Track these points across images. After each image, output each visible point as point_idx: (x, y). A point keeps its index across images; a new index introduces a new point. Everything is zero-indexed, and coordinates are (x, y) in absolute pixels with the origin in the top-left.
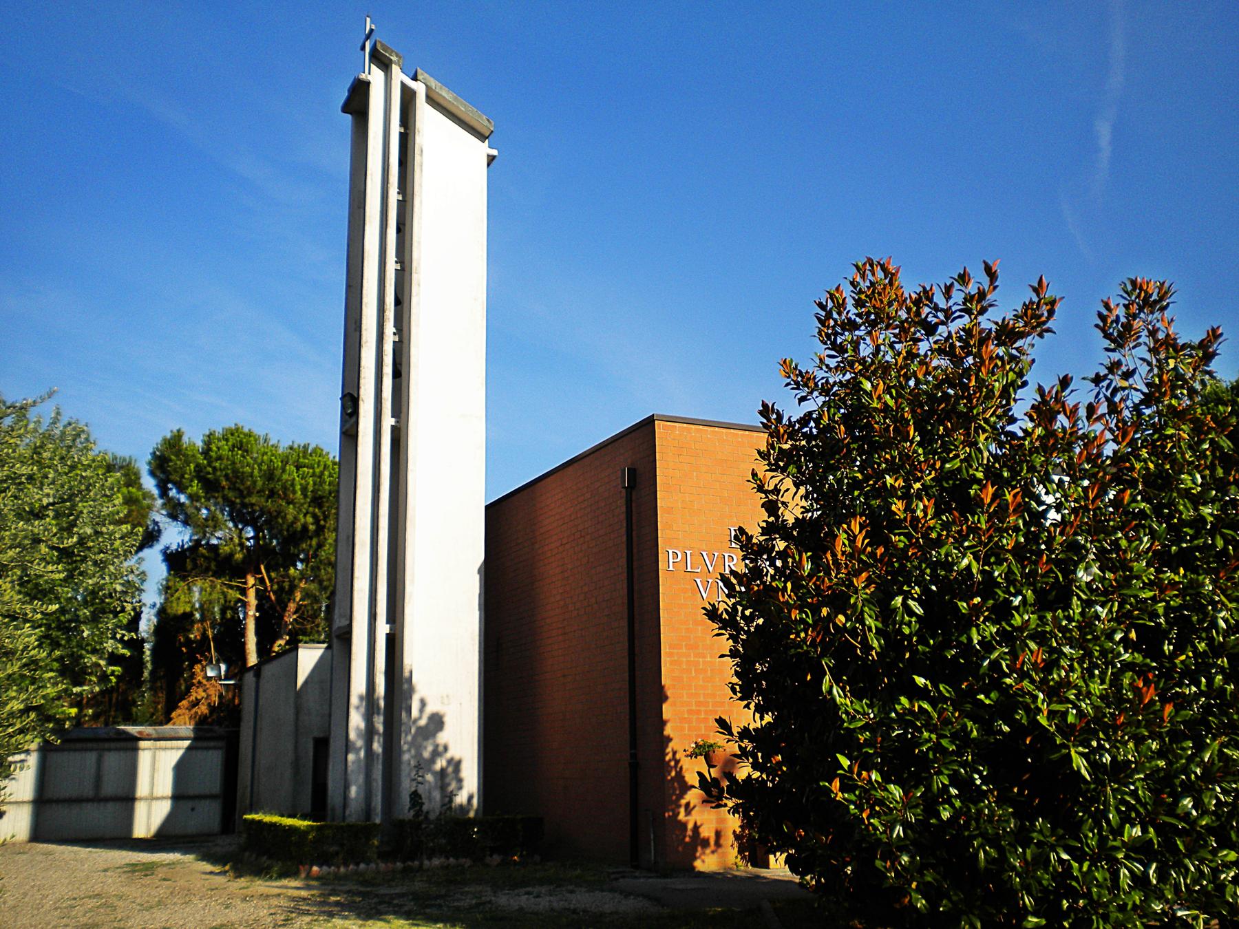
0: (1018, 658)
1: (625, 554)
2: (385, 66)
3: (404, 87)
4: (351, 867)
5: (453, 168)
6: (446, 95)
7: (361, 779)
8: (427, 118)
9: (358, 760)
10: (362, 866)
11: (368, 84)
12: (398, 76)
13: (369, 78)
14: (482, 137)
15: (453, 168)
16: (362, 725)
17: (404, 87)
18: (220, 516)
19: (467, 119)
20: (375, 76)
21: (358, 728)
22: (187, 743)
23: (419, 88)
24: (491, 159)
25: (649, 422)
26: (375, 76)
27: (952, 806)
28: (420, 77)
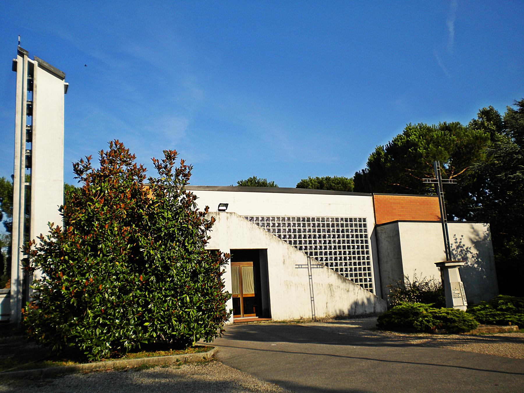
0: (76, 335)
2: (22, 55)
4: (4, 338)
7: (15, 308)
8: (40, 74)
9: (14, 302)
10: (8, 338)
14: (62, 78)
15: (50, 90)
16: (16, 289)
18: (110, 257)
20: (19, 59)
21: (14, 291)
22: (5, 295)
23: (35, 63)
24: (66, 87)
26: (19, 59)
27: (122, 226)
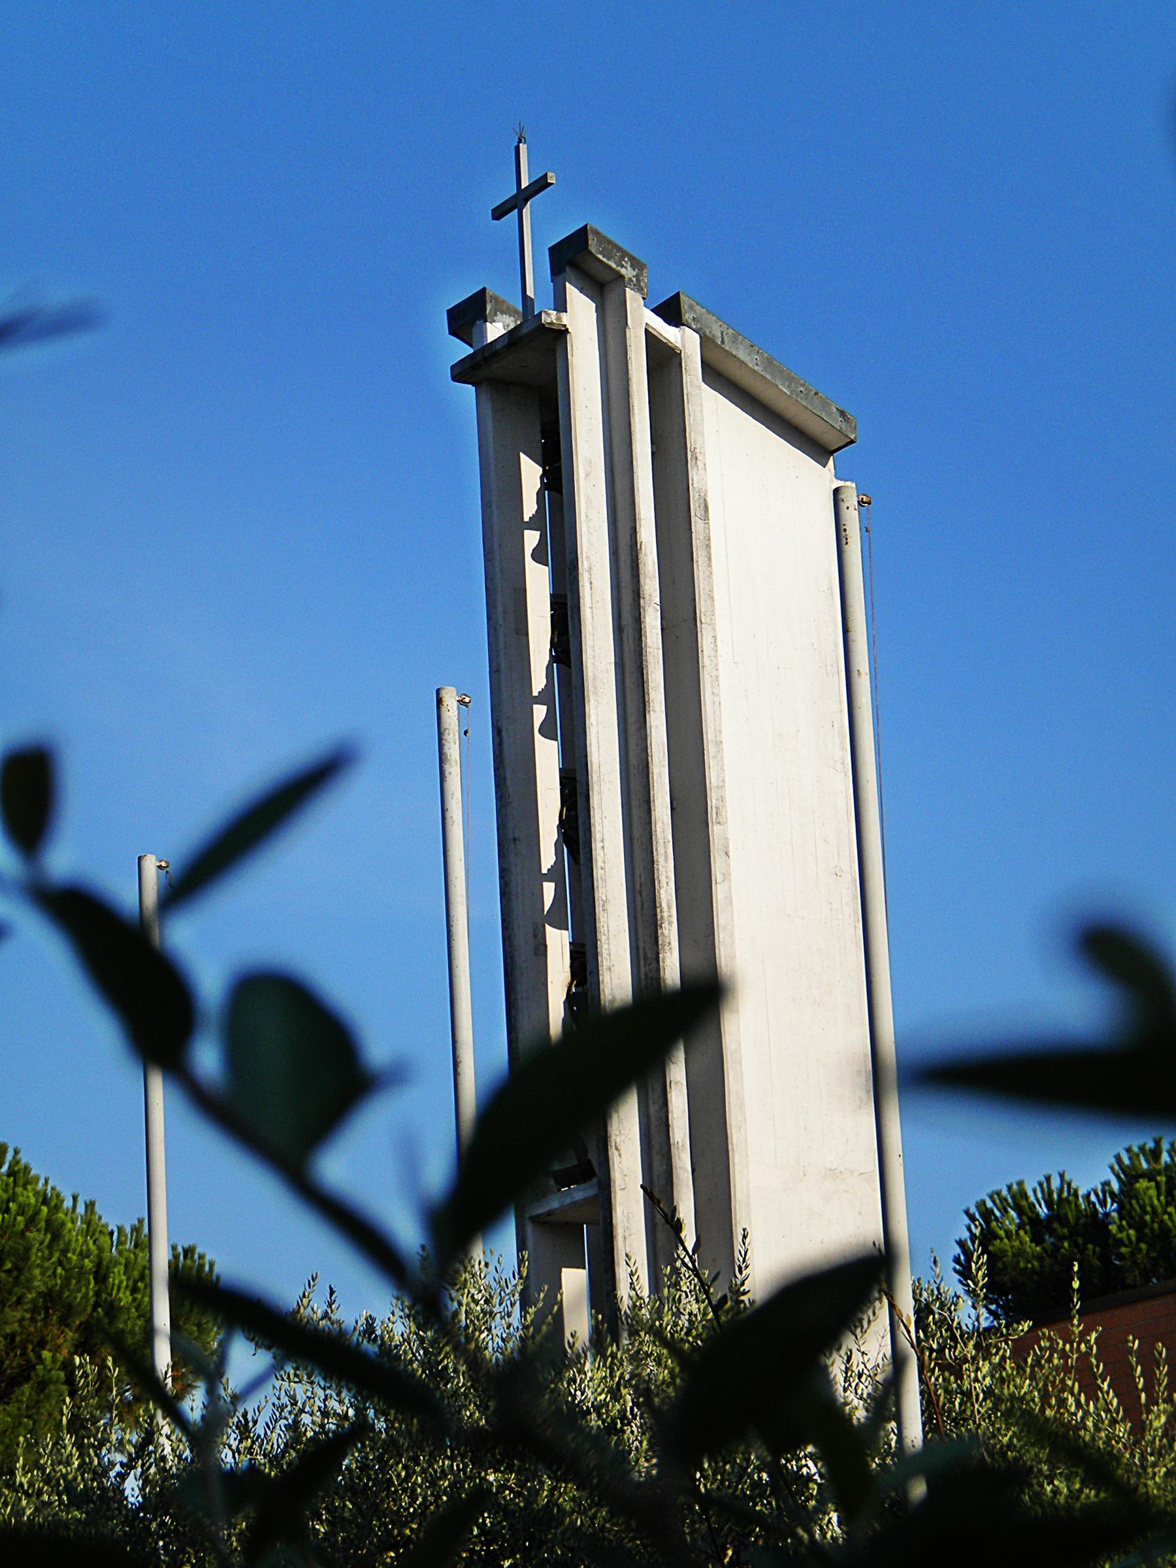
1: (888, 1329)
2: (604, 289)
3: (653, 342)
5: (768, 521)
6: (745, 358)
11: (560, 335)
12: (642, 318)
13: (565, 319)
15: (768, 521)
17: (653, 342)
19: (767, 395)
23: (684, 340)
25: (677, 296)
26: (580, 315)
28: (687, 316)
